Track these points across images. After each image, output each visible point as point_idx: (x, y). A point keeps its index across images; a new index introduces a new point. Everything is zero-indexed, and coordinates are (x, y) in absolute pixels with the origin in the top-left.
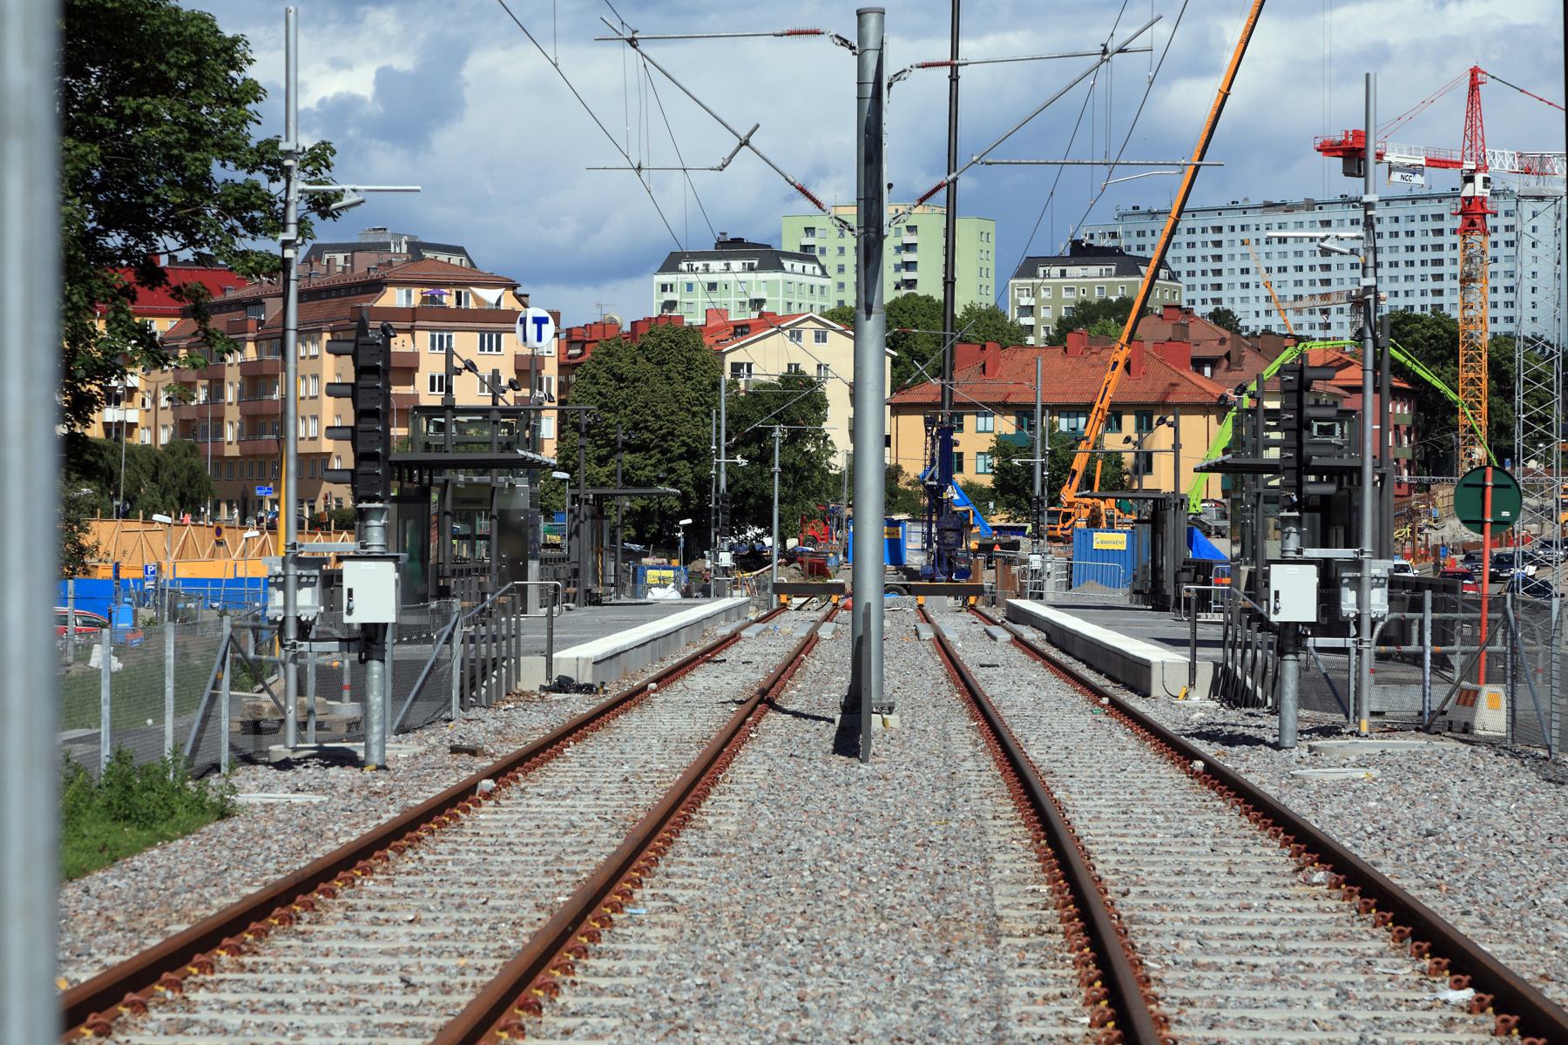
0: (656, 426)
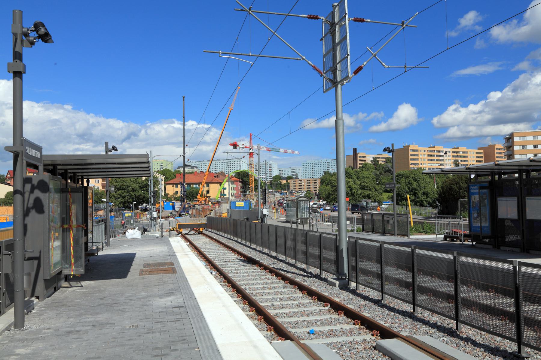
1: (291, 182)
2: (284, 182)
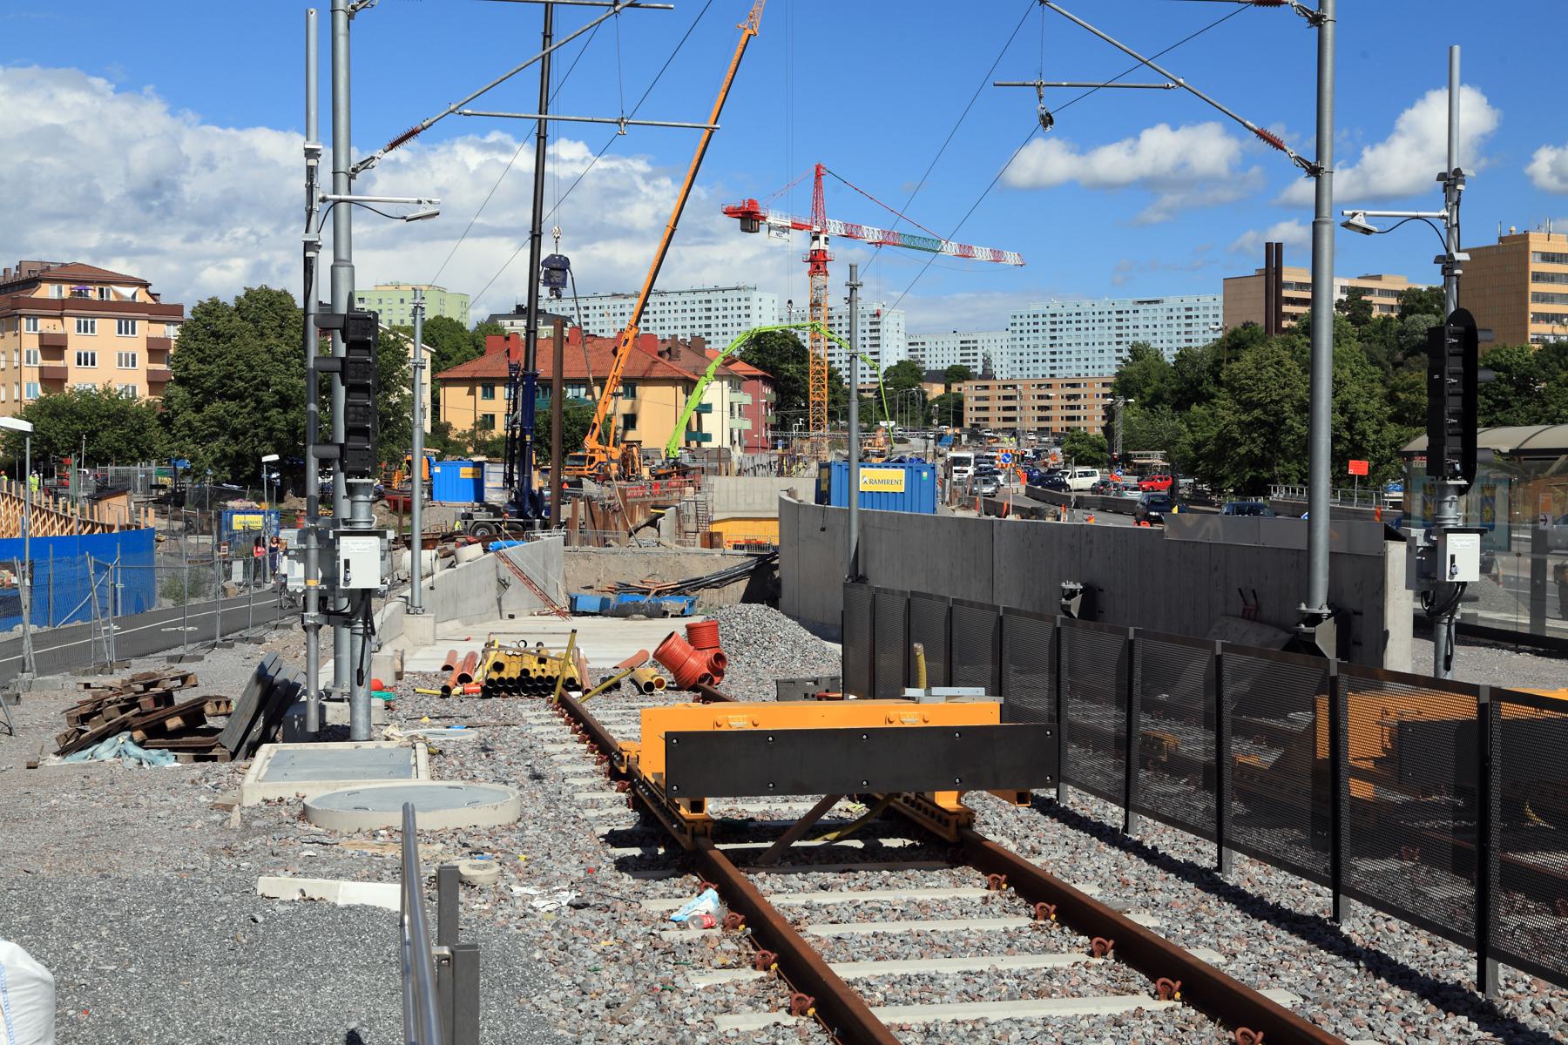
0: (249, 375)
1: (968, 390)
2: (936, 390)
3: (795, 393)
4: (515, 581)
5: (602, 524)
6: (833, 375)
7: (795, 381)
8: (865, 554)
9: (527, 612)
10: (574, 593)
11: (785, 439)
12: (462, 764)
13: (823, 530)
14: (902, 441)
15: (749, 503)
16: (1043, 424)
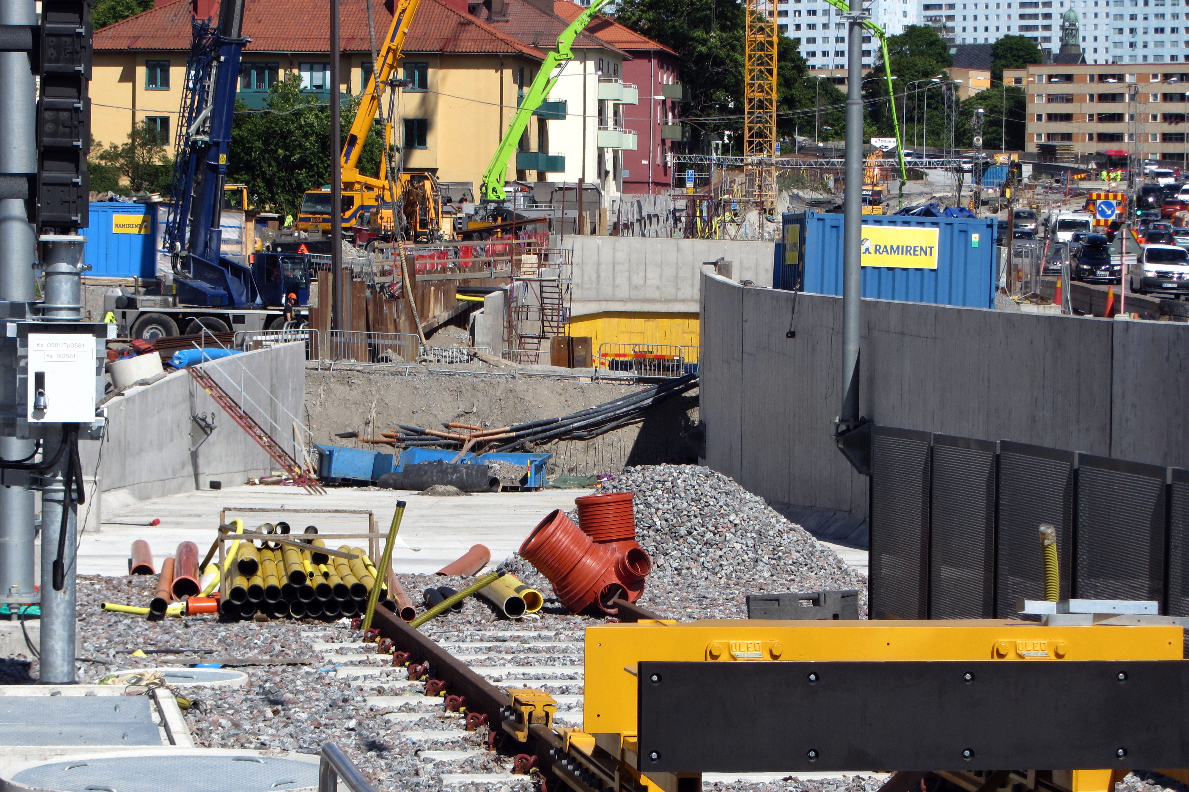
2: (977, 81)
3: (718, 83)
4: (223, 420)
5: (371, 322)
6: (788, 50)
7: (718, 62)
8: (871, 380)
9: (240, 478)
10: (325, 444)
11: (700, 168)
12: (236, 725)
13: (792, 335)
14: (916, 175)
15: (642, 283)
16: (1173, 148)
